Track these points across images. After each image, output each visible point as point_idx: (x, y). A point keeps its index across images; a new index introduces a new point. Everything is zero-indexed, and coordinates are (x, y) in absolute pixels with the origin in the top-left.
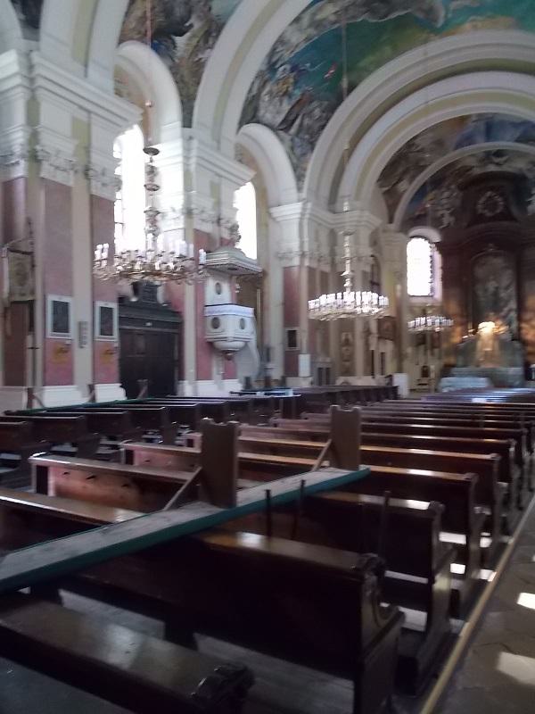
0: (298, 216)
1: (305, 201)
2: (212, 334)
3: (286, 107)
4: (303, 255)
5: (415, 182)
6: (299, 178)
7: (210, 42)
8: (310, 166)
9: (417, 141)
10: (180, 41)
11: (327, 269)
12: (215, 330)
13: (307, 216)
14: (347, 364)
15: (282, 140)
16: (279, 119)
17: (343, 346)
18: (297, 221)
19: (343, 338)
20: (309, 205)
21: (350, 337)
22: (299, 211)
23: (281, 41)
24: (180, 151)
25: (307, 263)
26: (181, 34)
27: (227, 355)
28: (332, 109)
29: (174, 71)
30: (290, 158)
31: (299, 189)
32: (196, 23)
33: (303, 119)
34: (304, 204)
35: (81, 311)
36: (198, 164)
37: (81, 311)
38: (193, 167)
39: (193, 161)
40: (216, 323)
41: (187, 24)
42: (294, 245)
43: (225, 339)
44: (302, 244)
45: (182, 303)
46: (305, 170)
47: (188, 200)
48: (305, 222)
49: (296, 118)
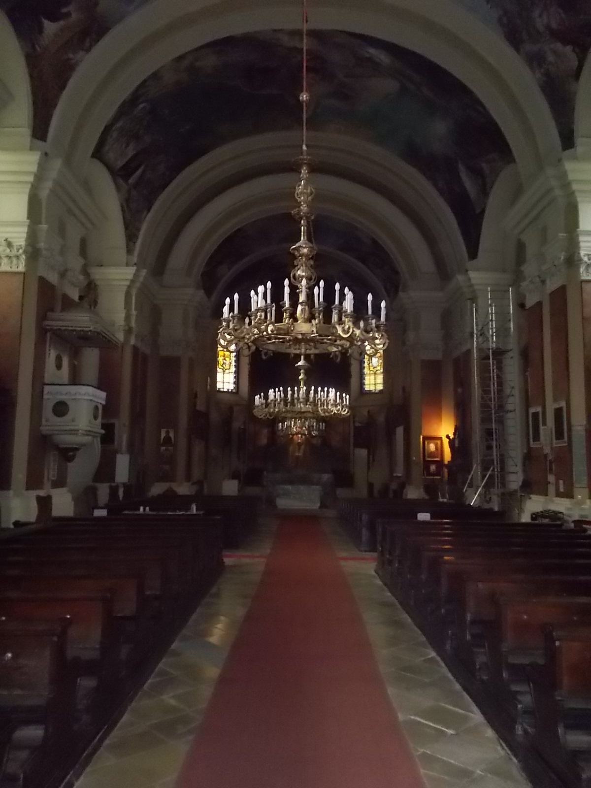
0: (128, 283)
1: (139, 265)
2: (50, 422)
3: (131, 152)
4: (129, 331)
5: (231, 271)
6: (131, 237)
7: (87, 44)
8: (144, 227)
9: (530, 302)
10: (50, 28)
11: (148, 351)
12: (58, 420)
13: (138, 285)
14: (167, 467)
15: (118, 188)
16: (120, 163)
17: (163, 445)
18: (125, 289)
19: (163, 435)
20: (144, 272)
21: (172, 435)
22: (130, 277)
23: (155, 76)
24: (34, 168)
25: (133, 341)
26: (54, 18)
27: (67, 454)
28: (177, 169)
29: (32, 60)
30: (123, 211)
31: (129, 251)
32: (74, 14)
33: (144, 172)
34: (137, 270)
35: (93, 484)
36: (53, 191)
37: (93, 484)
38: (44, 194)
39: (48, 185)
40: (61, 409)
41: (64, 10)
42: (120, 317)
43: (74, 432)
44: (128, 318)
45: (15, 378)
46: (139, 230)
47: (32, 237)
48: (134, 292)
49: (139, 166)
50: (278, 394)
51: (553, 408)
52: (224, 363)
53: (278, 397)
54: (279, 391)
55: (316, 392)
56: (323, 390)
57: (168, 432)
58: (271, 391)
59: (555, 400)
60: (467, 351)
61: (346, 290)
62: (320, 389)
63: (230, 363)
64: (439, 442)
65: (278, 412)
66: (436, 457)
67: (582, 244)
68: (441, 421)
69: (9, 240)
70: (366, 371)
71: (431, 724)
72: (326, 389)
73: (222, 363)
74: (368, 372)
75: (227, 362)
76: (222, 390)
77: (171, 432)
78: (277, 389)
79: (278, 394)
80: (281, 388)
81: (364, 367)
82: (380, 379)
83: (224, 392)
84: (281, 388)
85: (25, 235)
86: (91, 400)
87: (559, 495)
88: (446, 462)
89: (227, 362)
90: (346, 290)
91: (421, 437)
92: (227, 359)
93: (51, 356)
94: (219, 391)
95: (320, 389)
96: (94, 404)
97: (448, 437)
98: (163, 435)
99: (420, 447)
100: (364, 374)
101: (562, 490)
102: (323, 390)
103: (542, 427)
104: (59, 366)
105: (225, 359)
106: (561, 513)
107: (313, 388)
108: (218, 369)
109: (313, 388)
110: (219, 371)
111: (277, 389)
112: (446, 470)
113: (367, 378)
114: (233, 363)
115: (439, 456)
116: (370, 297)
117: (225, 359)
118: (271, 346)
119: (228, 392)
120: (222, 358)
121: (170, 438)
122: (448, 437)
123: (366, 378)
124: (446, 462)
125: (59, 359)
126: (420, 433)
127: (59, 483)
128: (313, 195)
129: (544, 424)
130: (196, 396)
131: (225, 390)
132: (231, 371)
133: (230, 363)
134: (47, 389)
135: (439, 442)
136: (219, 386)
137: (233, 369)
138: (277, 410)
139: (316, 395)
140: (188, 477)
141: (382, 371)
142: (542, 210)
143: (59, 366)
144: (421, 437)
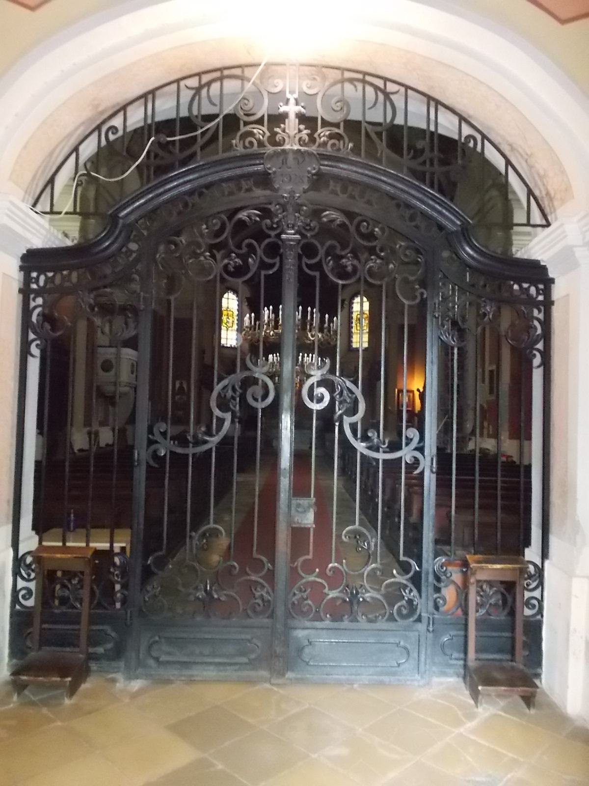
21: (185, 386)
27: (109, 400)
40: (107, 366)
50: (275, 358)
52: (227, 322)
54: (277, 356)
55: (303, 357)
56: (308, 356)
57: (181, 384)
58: (270, 356)
59: (491, 363)
62: (306, 355)
63: (233, 322)
65: (275, 372)
67: (514, 242)
68: (414, 379)
69: (66, 232)
70: (354, 330)
71: (151, 196)
72: (310, 355)
73: (226, 321)
74: (356, 331)
75: (230, 321)
76: (225, 345)
77: (184, 382)
78: (275, 355)
79: (275, 358)
80: (278, 354)
81: (352, 327)
82: (366, 338)
83: (227, 347)
84: (278, 354)
85: (78, 229)
86: (130, 359)
87: (489, 436)
88: (417, 412)
89: (230, 321)
91: (396, 390)
92: (230, 317)
94: (223, 346)
95: (306, 355)
96: (132, 361)
97: (418, 390)
98: (177, 385)
99: (394, 401)
100: (352, 332)
101: (491, 433)
102: (308, 356)
105: (228, 318)
106: (487, 449)
107: (301, 354)
108: (222, 327)
109: (301, 354)
110: (223, 328)
111: (275, 355)
112: (416, 418)
113: (354, 336)
114: (236, 322)
115: (411, 406)
116: (327, 316)
117: (228, 318)
118: (271, 339)
119: (231, 348)
120: (226, 317)
121: (183, 388)
122: (418, 390)
123: (354, 336)
124: (417, 412)
126: (396, 386)
127: (103, 423)
131: (229, 346)
132: (233, 328)
133: (233, 322)
135: (411, 395)
136: (223, 342)
137: (235, 327)
138: (274, 370)
139: (331, 325)
141: (367, 330)
144: (396, 390)
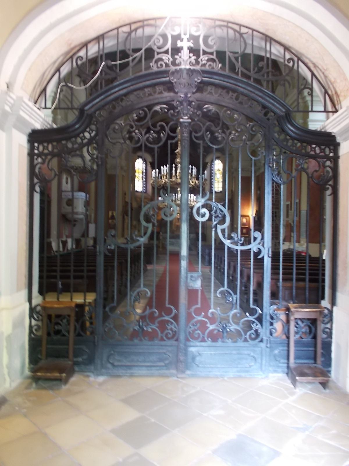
19: (110, 214)
40: (70, 202)
51: (129, 247)
53: (9, 99)
57: (113, 213)
60: (137, 322)
61: (193, 167)
64: (248, 218)
66: (246, 225)
90: (193, 167)
93: (64, 177)
98: (110, 214)
103: (290, 211)
104: (67, 183)
125: (67, 179)
128: (196, 188)
129: (291, 210)
130: (125, 194)
134: (63, 194)
140: (123, 236)
142: (134, 366)
143: (67, 183)
